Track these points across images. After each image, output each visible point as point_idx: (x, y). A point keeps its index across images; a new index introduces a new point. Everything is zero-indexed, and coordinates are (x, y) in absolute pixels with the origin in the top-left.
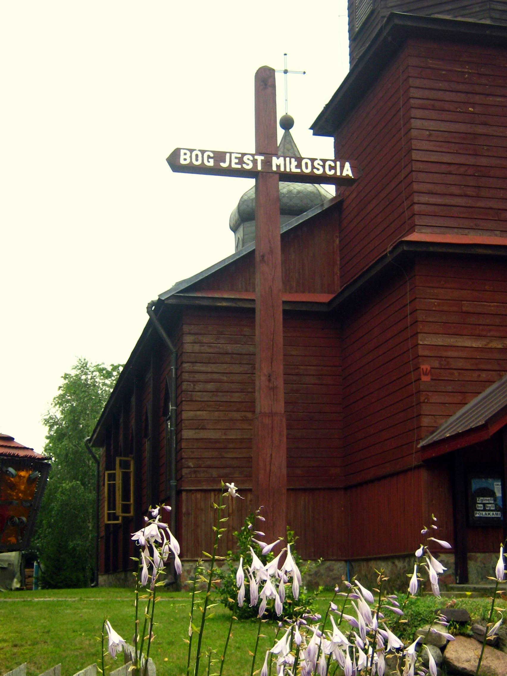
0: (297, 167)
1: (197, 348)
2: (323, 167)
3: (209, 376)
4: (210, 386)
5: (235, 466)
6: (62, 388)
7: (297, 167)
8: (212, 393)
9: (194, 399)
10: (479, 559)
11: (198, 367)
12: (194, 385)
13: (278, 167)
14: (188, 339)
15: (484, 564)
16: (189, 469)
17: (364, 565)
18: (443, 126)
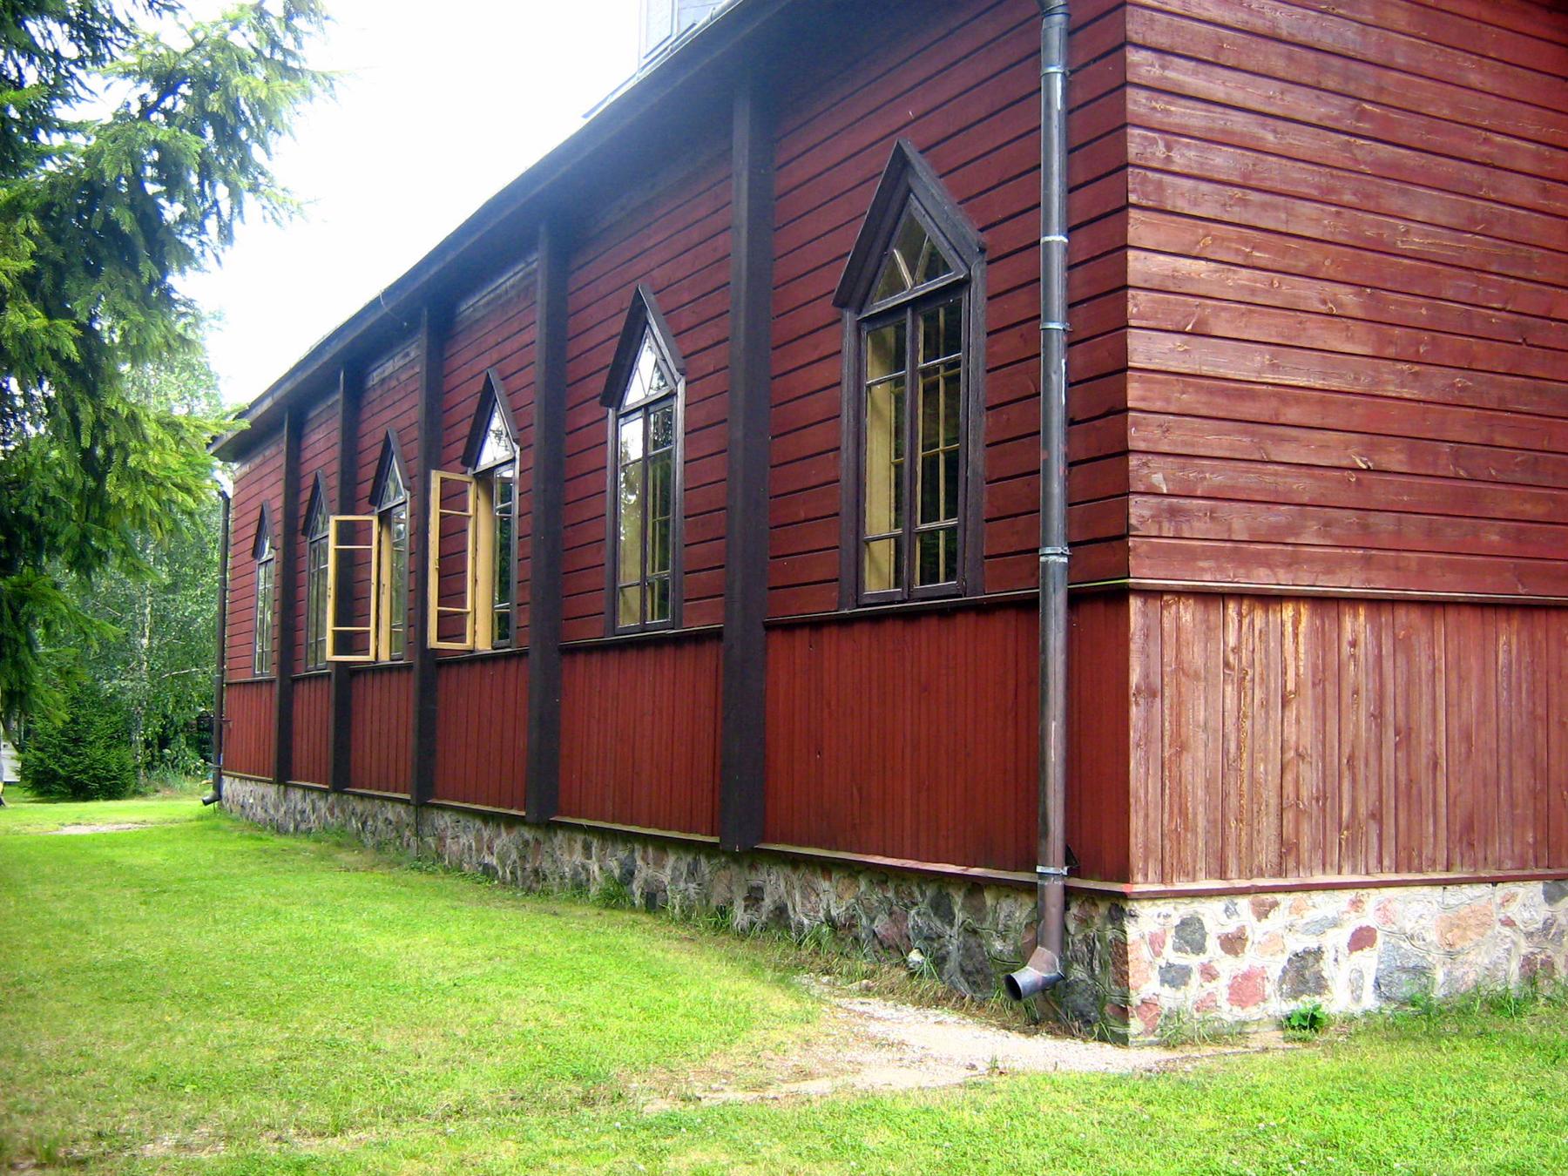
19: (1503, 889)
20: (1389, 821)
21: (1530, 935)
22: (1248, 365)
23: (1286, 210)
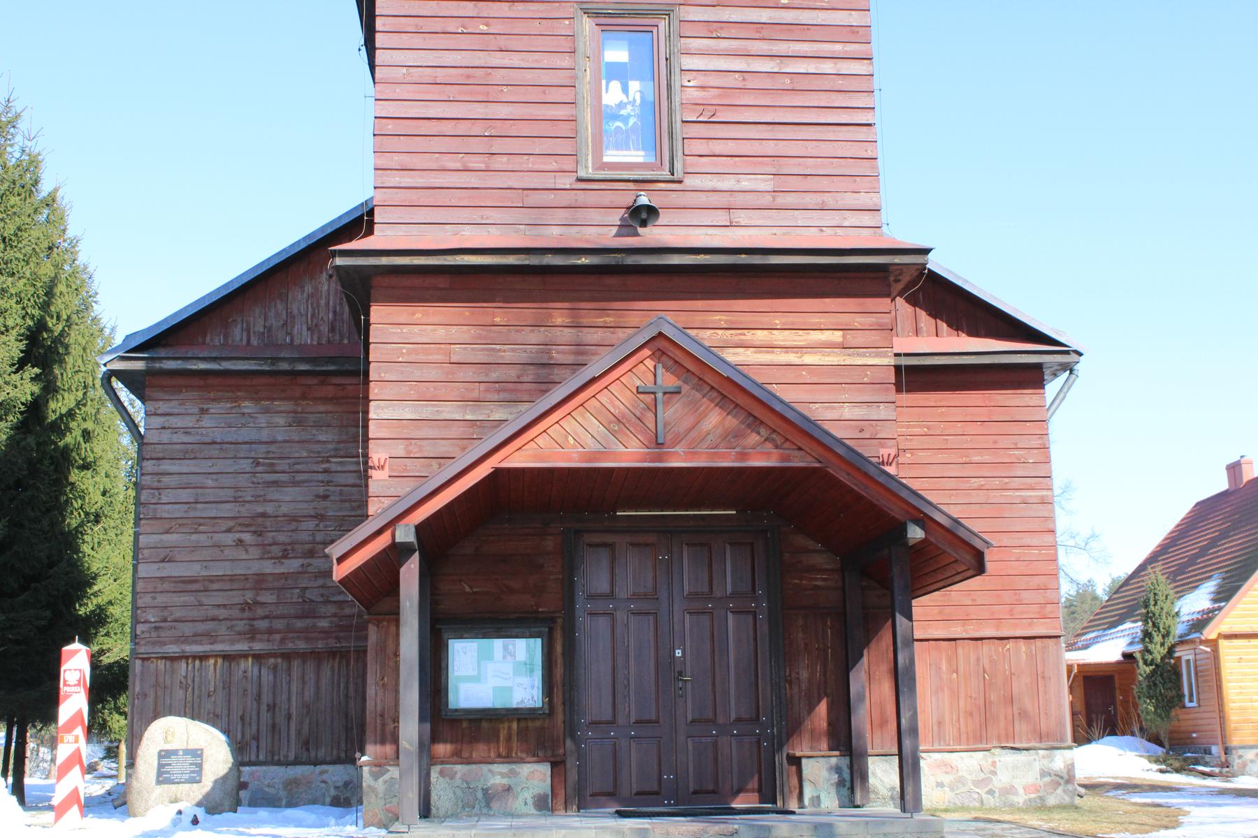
3: (185, 479)
4: (185, 495)
5: (221, 618)
8: (188, 506)
9: (158, 516)
10: (459, 775)
11: (166, 466)
12: (160, 494)
15: (467, 783)
16: (147, 625)
17: (181, 794)
19: (319, 768)
20: (263, 744)
21: (336, 788)
22: (194, 570)
23: (216, 509)
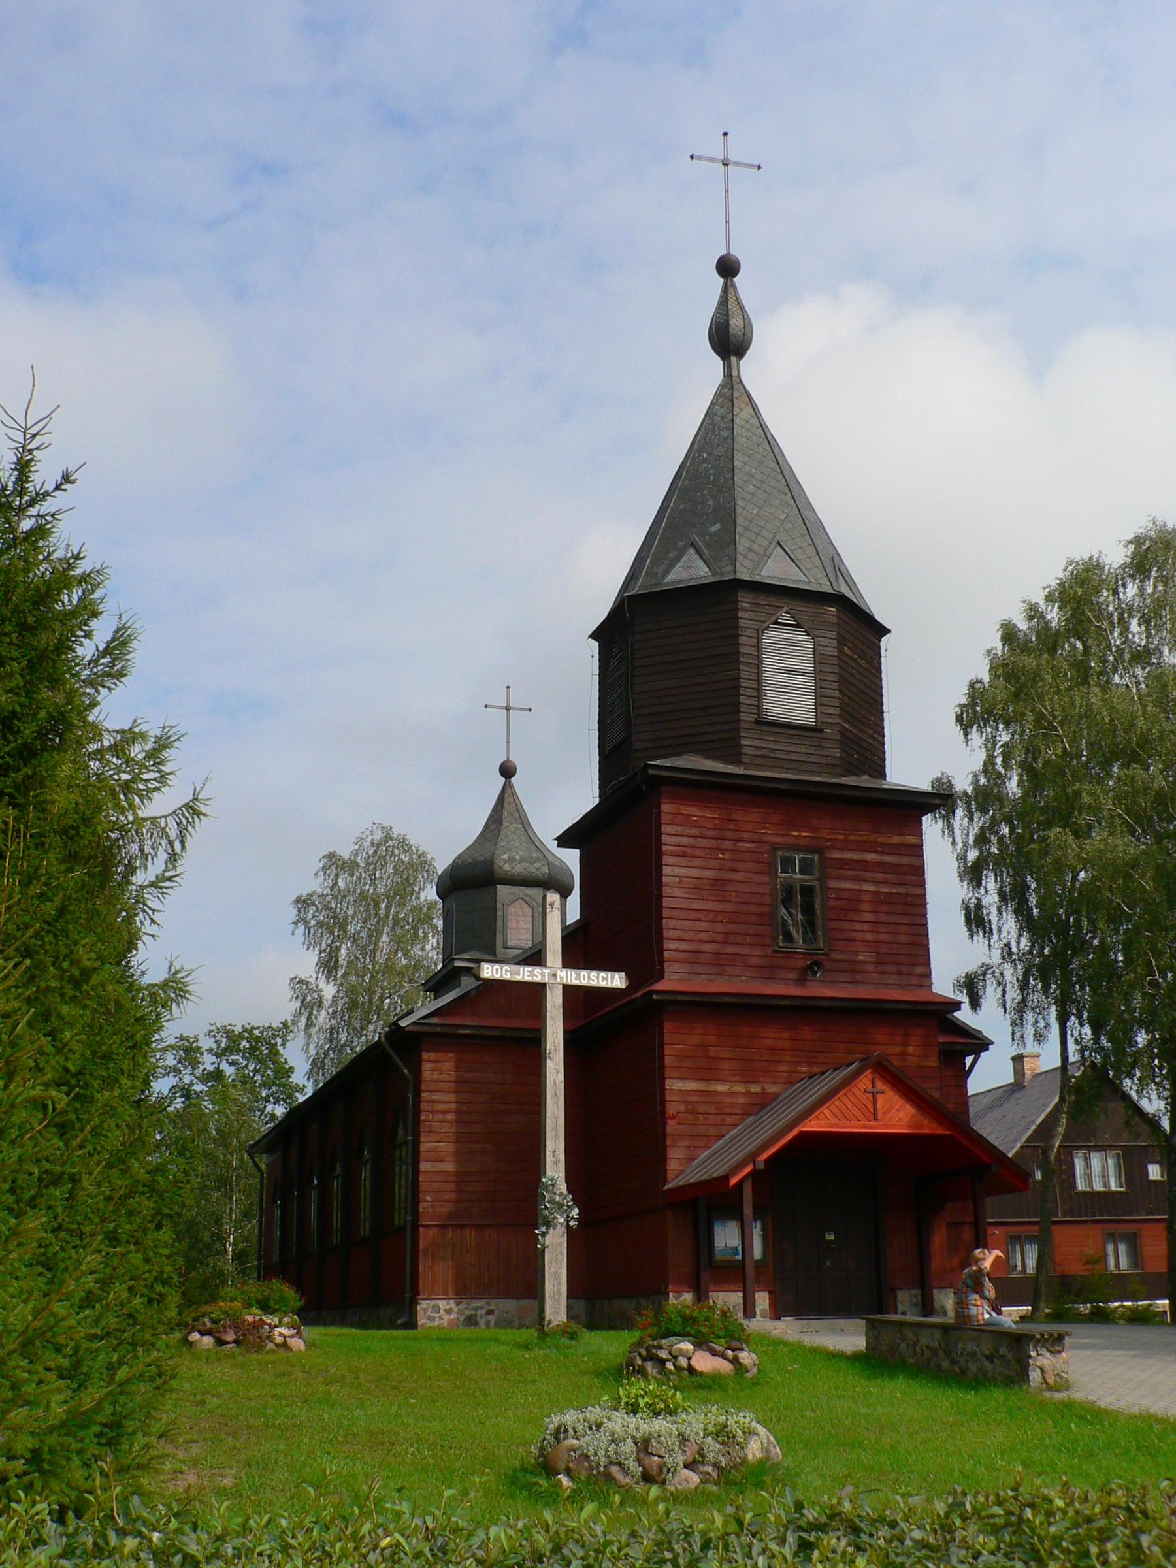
0: (576, 979)
1: (436, 1075)
2: (598, 978)
6: (1059, 1380)
7: (576, 979)
13: (562, 978)
14: (426, 1066)
18: (693, 872)
